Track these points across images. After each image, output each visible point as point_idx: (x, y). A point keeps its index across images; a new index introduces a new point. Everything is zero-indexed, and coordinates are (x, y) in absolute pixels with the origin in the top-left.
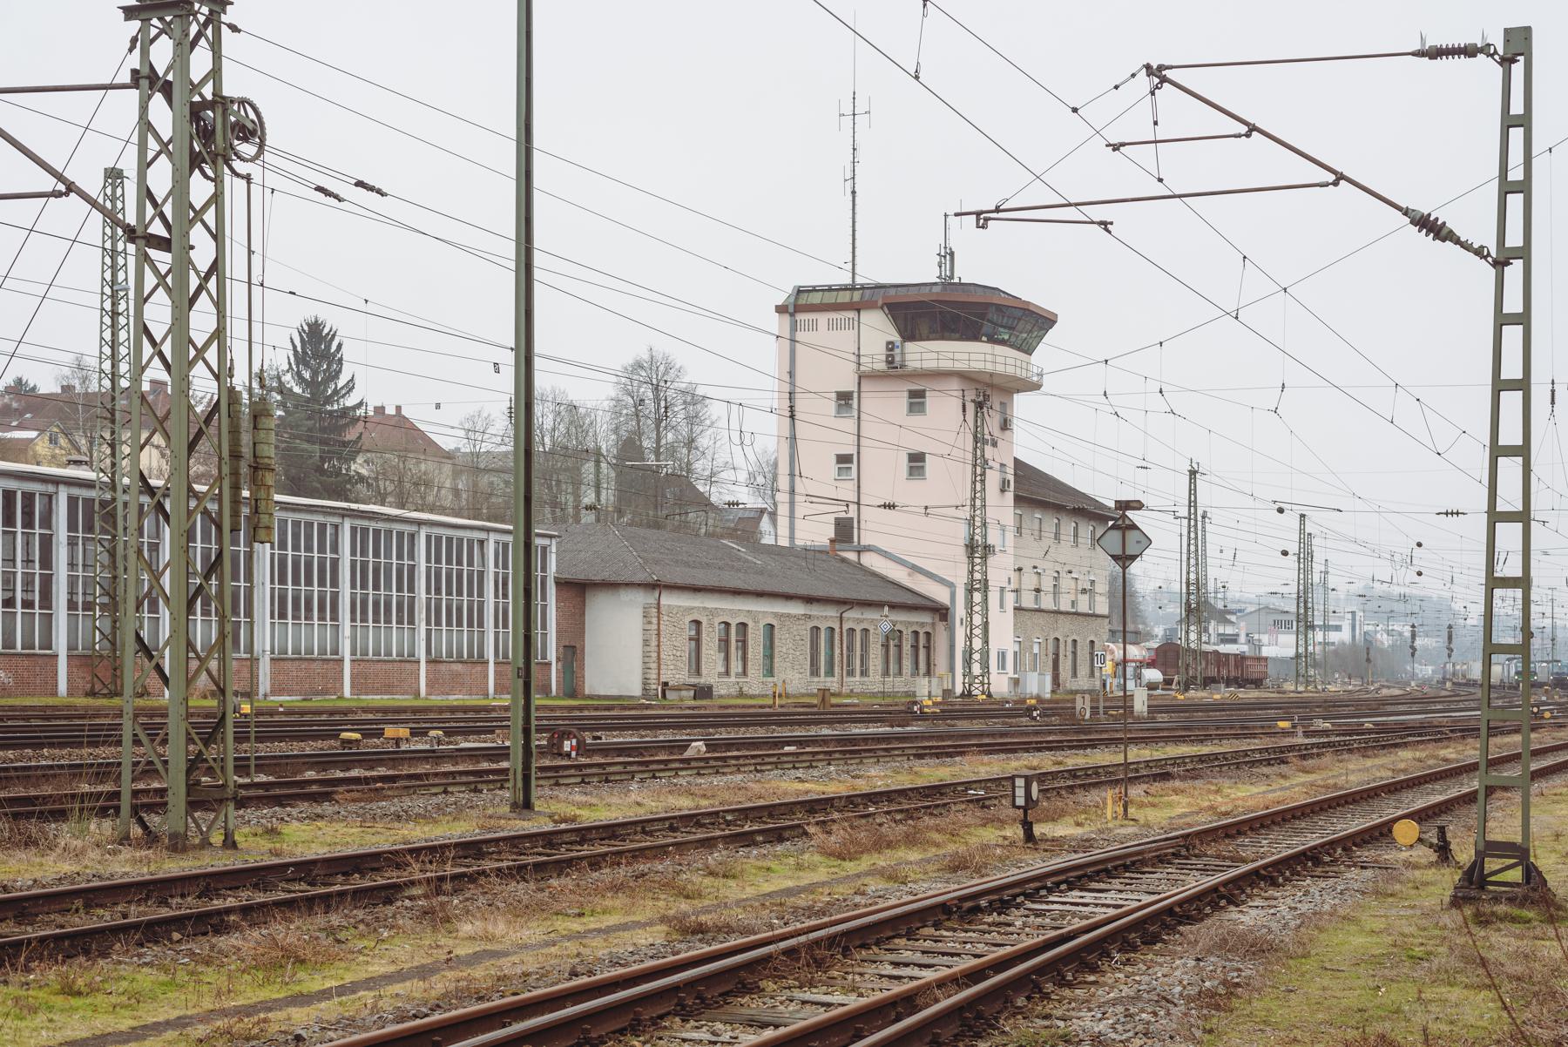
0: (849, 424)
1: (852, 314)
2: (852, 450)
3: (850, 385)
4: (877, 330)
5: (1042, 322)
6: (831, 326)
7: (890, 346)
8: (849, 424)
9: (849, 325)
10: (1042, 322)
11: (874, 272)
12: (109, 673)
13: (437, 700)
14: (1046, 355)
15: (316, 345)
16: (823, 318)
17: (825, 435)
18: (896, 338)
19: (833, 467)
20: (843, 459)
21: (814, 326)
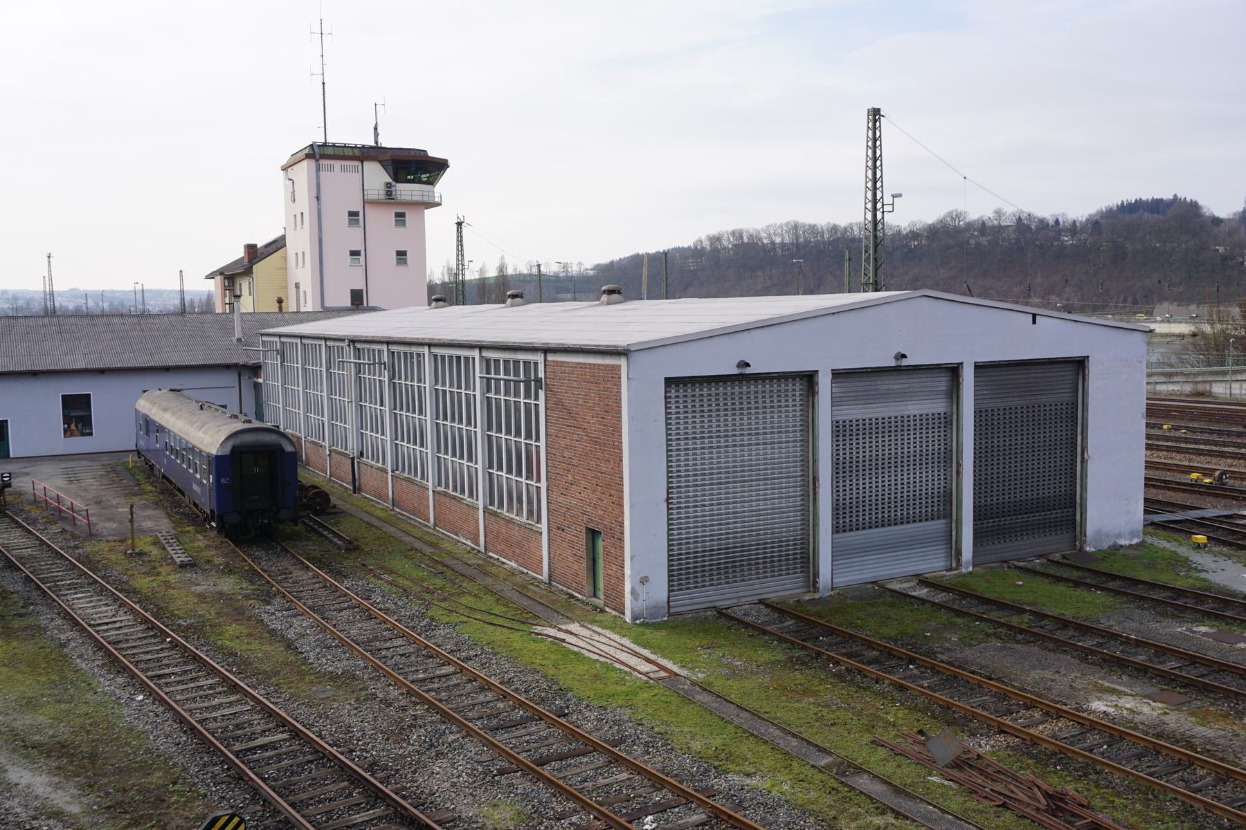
0: (358, 231)
1: (357, 163)
2: (360, 247)
3: (357, 207)
4: (377, 176)
5: (440, 166)
6: (343, 169)
7: (388, 185)
8: (358, 231)
9: (355, 169)
10: (440, 166)
11: (387, 142)
12: (573, 784)
13: (844, 579)
14: (443, 187)
15: (211, 276)
16: (337, 164)
17: (344, 237)
18: (390, 180)
19: (349, 258)
20: (355, 253)
21: (332, 169)
